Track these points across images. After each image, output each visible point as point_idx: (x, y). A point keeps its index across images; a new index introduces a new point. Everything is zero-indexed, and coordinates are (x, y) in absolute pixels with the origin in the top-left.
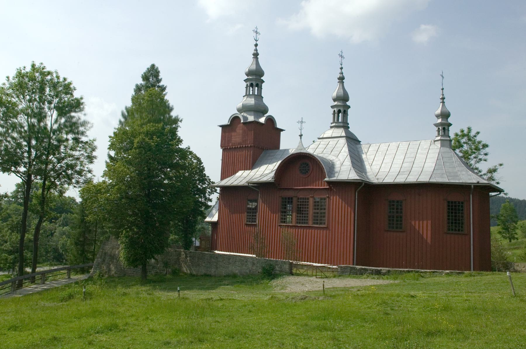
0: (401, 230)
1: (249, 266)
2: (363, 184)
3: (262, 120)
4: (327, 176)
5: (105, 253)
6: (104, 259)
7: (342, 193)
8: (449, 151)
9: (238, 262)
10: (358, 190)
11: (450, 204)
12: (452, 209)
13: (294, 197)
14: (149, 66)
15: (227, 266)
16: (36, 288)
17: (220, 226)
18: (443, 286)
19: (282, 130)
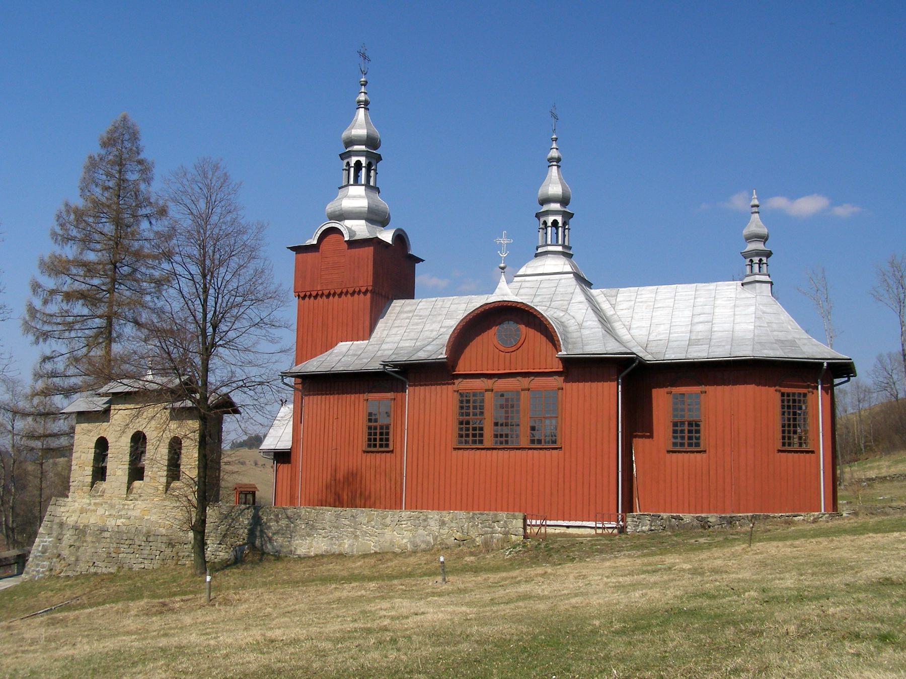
1: (433, 529)
3: (387, 236)
4: (562, 348)
5: (61, 525)
8: (773, 303)
9: (405, 523)
11: (785, 398)
12: (789, 407)
14: (119, 117)
17: (299, 459)
19: (419, 260)
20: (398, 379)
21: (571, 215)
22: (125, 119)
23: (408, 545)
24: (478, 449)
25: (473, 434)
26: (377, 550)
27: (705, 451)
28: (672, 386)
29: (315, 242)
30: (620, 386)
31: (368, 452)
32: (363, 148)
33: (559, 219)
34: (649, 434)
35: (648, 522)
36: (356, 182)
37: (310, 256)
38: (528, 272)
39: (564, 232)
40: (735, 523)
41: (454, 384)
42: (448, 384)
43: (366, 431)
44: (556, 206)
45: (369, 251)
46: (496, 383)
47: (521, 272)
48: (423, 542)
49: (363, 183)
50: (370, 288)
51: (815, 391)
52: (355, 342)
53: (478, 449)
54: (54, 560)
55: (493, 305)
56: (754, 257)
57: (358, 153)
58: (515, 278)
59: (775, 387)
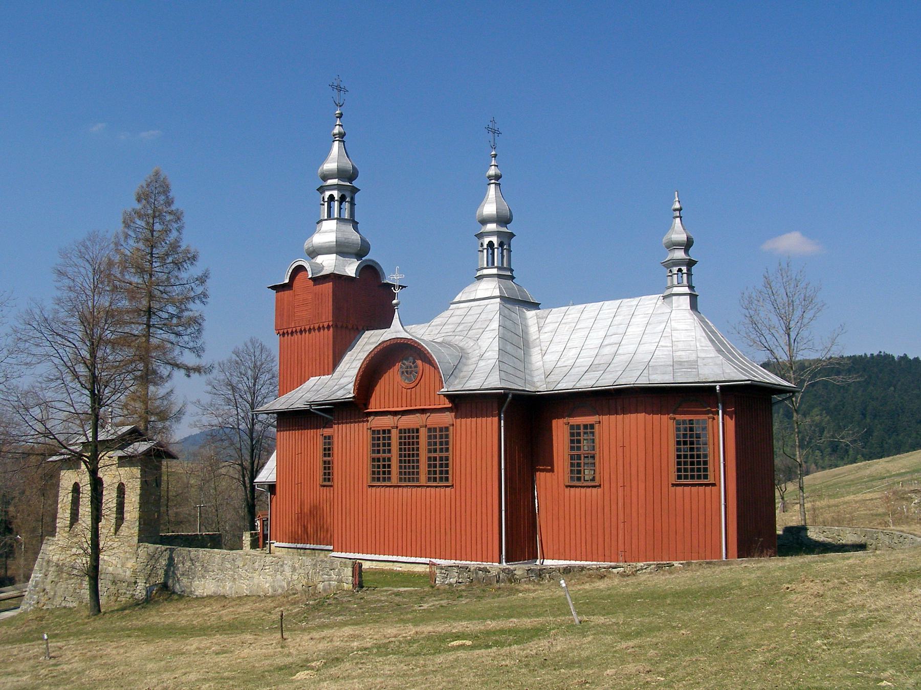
0: (706, 481)
2: (510, 396)
5: (49, 562)
6: (47, 573)
7: (476, 413)
10: (504, 409)
13: (393, 428)
15: (250, 575)
16: (353, 637)
18: (896, 599)
20: (321, 416)
21: (512, 235)
22: (157, 174)
23: (270, 590)
24: (387, 486)
25: (580, 436)
26: (248, 593)
27: (600, 486)
28: (570, 416)
29: (287, 281)
30: (502, 421)
31: (324, 486)
32: (335, 181)
33: (495, 240)
34: (549, 468)
35: (456, 574)
36: (330, 217)
37: (287, 293)
38: (463, 299)
39: (502, 253)
40: (545, 576)
41: (368, 421)
42: (363, 421)
43: (322, 465)
44: (492, 227)
45: (328, 286)
46: (400, 420)
47: (456, 299)
48: (280, 586)
49: (336, 216)
50: (331, 323)
51: (716, 417)
52: (322, 377)
53: (387, 486)
54: (41, 594)
55: (389, 342)
56: (672, 267)
57: (331, 187)
58: (451, 305)
59: (668, 415)
